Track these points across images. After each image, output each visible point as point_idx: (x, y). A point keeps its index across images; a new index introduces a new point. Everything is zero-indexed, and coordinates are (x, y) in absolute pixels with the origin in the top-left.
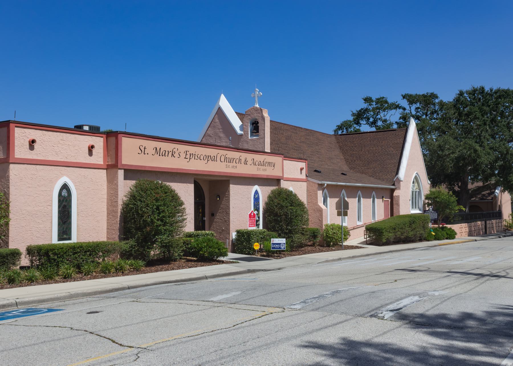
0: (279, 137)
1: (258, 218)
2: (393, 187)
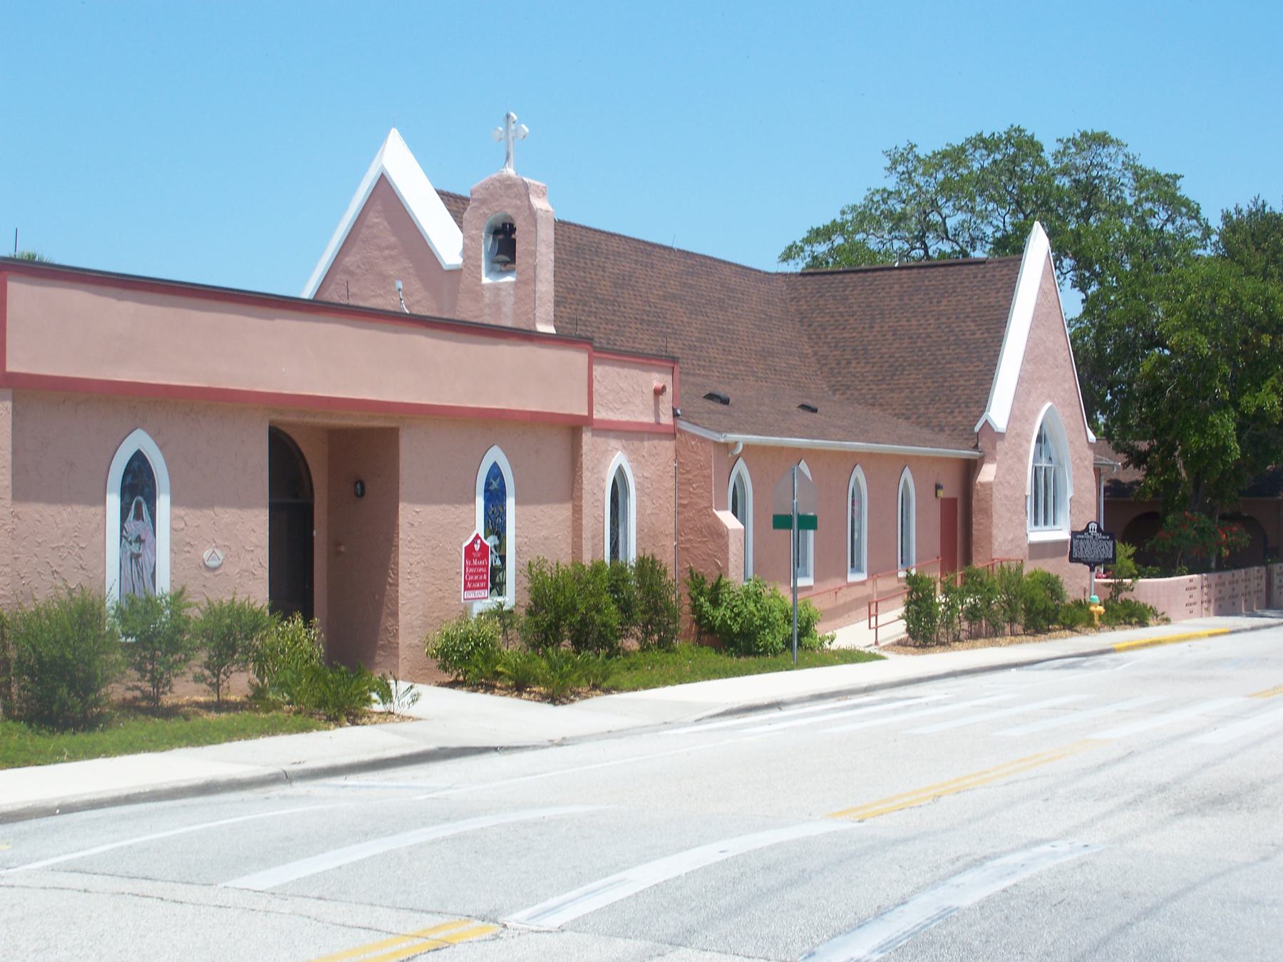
0: (589, 280)
1: (498, 560)
2: (975, 454)
